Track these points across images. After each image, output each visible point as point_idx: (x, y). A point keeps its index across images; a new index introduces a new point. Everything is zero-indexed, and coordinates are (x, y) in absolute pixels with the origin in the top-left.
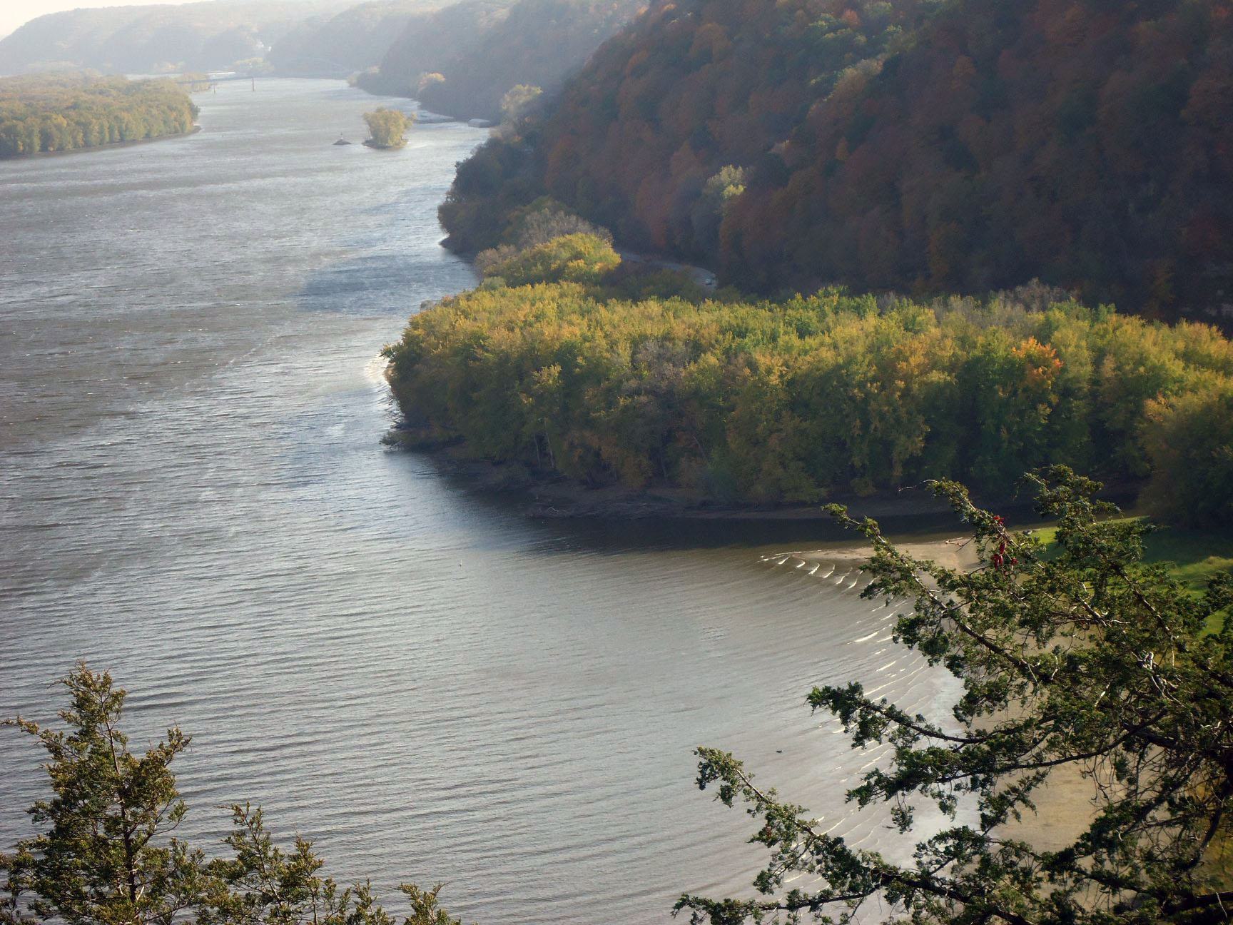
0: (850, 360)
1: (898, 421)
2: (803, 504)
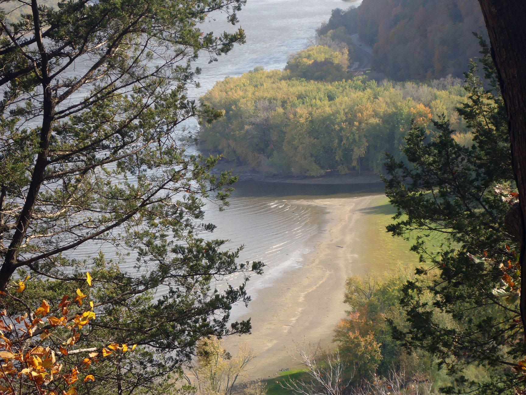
0: (338, 112)
1: (354, 140)
2: (313, 177)
